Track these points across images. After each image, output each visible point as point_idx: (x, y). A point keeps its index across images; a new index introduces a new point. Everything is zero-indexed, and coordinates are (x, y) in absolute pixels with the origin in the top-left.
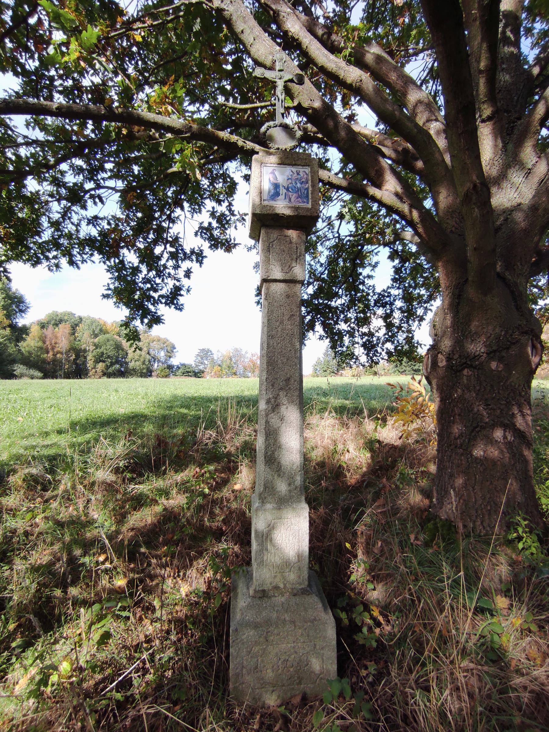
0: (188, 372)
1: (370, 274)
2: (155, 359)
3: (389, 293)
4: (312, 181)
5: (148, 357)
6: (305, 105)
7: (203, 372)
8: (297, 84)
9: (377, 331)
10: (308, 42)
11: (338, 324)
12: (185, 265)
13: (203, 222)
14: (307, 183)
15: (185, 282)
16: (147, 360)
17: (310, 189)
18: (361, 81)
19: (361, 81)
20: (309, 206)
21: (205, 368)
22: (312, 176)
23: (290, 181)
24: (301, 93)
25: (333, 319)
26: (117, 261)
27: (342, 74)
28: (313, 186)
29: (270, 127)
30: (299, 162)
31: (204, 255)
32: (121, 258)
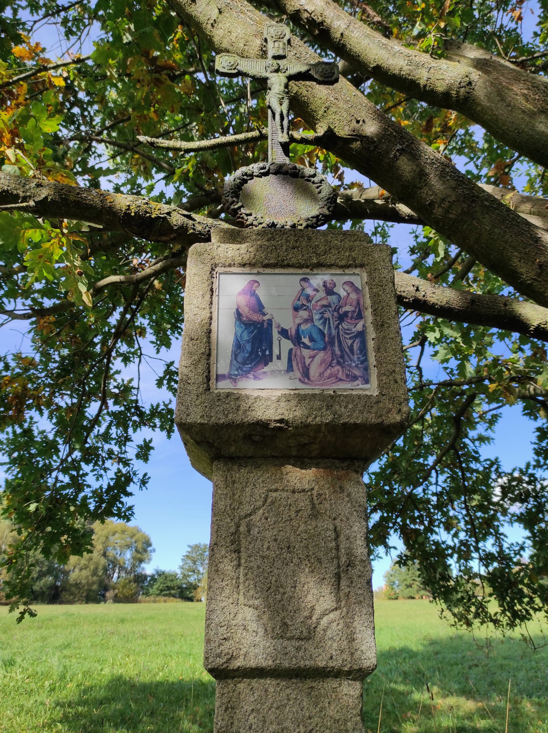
0: (169, 588)
1: (484, 434)
2: (114, 563)
3: (532, 475)
4: (375, 312)
5: (103, 561)
6: (343, 131)
7: (195, 587)
8: (320, 83)
9: (517, 553)
10: (343, 26)
11: (432, 532)
12: (140, 435)
13: (172, 363)
14: (360, 316)
15: (138, 466)
16: (101, 567)
17: (371, 334)
18: (470, 83)
19: (470, 83)
20: (372, 389)
21: (199, 580)
22: (374, 296)
23: (304, 314)
24: (332, 109)
25: (422, 523)
26: (19, 431)
27: (423, 76)
29: (251, 176)
30: (330, 258)
32: (26, 425)
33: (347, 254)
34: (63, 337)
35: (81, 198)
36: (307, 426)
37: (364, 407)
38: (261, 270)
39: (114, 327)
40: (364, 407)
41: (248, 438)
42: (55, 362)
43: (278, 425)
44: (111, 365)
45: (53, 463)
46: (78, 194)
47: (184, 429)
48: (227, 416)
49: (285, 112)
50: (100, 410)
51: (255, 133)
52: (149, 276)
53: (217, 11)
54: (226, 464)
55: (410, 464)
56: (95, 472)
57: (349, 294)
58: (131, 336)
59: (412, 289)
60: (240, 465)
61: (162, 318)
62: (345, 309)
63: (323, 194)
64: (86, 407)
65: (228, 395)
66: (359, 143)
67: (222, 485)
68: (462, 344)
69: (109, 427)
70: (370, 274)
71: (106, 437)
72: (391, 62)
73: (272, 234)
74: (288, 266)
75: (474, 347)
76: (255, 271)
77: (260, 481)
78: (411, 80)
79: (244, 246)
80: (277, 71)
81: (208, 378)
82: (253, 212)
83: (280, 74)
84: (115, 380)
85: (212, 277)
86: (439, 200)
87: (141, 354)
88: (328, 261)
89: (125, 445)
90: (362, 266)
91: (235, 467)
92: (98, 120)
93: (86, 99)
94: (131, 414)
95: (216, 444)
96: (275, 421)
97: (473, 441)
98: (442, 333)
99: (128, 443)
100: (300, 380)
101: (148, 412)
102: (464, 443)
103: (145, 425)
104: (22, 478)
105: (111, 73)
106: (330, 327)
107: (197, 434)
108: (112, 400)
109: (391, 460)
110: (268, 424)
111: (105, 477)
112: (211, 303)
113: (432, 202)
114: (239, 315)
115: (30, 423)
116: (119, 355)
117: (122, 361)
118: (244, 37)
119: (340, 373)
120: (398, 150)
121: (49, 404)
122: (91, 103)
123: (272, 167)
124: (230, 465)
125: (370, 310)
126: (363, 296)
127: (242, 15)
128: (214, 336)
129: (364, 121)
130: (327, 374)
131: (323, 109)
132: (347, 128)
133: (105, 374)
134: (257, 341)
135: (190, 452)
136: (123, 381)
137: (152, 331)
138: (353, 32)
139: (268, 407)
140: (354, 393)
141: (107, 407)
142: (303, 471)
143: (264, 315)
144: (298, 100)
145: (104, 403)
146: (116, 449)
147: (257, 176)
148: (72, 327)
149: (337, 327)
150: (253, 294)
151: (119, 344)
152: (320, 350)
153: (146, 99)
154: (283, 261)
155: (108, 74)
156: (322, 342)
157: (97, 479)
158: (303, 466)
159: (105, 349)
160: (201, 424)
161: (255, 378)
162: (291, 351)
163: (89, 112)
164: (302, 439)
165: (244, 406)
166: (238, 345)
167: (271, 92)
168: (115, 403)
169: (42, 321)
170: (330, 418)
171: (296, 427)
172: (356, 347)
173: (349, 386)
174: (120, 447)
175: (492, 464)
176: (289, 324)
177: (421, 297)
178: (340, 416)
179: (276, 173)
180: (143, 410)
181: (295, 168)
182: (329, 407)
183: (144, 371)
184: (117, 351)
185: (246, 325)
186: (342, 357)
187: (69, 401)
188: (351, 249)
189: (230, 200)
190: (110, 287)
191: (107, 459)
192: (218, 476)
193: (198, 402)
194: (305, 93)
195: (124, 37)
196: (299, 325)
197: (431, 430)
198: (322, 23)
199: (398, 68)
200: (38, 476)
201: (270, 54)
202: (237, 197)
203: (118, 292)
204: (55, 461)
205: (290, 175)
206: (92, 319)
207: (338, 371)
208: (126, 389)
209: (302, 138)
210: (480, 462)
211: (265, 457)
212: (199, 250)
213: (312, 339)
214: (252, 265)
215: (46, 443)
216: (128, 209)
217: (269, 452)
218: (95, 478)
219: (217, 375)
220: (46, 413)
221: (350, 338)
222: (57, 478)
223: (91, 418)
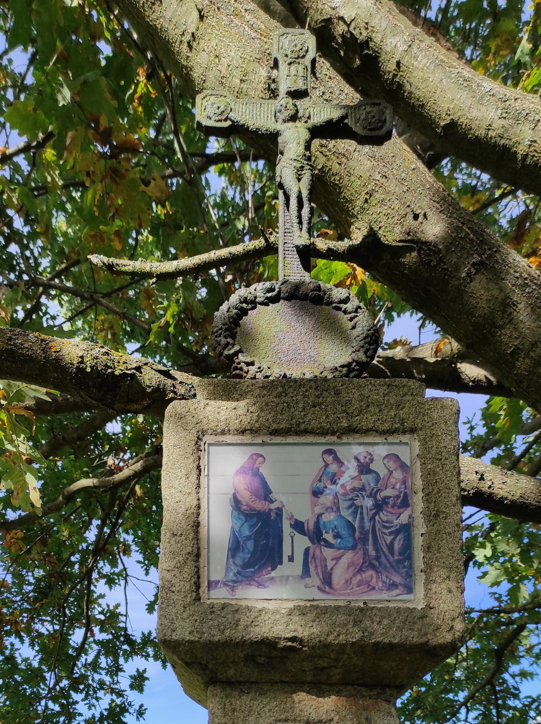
4: (427, 496)
6: (391, 236)
8: (362, 140)
12: (132, 665)
14: (405, 503)
15: (133, 696)
17: (420, 527)
22: (429, 476)
24: (378, 196)
28: (433, 516)
29: (254, 303)
30: (368, 420)
31: (136, 673)
32: (7, 652)
33: (392, 413)
34: (34, 554)
35: (15, 345)
36: (327, 646)
37: (404, 623)
38: (267, 439)
39: (92, 544)
40: (404, 623)
41: (251, 659)
42: (30, 584)
43: (290, 644)
44: (92, 588)
45: (41, 691)
46: (10, 339)
47: (169, 648)
48: (223, 632)
49: (305, 193)
50: (85, 638)
51: (259, 243)
52: (128, 479)
53: (196, 14)
54: (224, 689)
55: (437, 699)
56: (87, 702)
57: (391, 472)
58: (114, 555)
59: (475, 477)
60: (242, 691)
61: (149, 533)
62: (384, 494)
63: (358, 330)
64: (70, 635)
65: (224, 607)
66: (414, 254)
67: (219, 713)
68: (519, 563)
69: (97, 656)
70: (424, 443)
71: (95, 666)
72: (474, 113)
73: (283, 387)
74: (306, 432)
75: (535, 566)
76: (259, 440)
77: (266, 709)
78: (504, 146)
79: (242, 403)
80: (294, 118)
81: (198, 586)
82: (256, 359)
83: (298, 123)
84: (100, 605)
85: (199, 450)
86: (527, 345)
87: (127, 575)
88: (364, 425)
89: (117, 675)
90: (412, 431)
91: (236, 693)
92: (45, 262)
93: (26, 230)
94: (120, 643)
95: (210, 666)
96: (285, 639)
97: (513, 676)
98: (494, 549)
99: (119, 673)
100: (319, 588)
101: (139, 640)
102: (503, 679)
103: (137, 654)
104: (11, 706)
105: (53, 179)
106: (362, 518)
107: (186, 653)
108: (98, 627)
109: (415, 695)
110: (276, 643)
111: (98, 707)
112: (199, 486)
113: (517, 348)
114: (236, 503)
115: (12, 649)
116: (102, 576)
117: (106, 584)
118: (238, 62)
119: (374, 580)
120: (474, 264)
121: (29, 630)
122: (33, 236)
123: (283, 288)
124: (229, 691)
125: (420, 494)
126: (413, 475)
127: (236, 21)
128: (203, 530)
129: (425, 216)
130: (356, 580)
131: (363, 196)
132: (398, 229)
133: (87, 598)
134: (262, 539)
135: (180, 677)
136: (108, 606)
137: (137, 549)
138: (416, 58)
139: (276, 622)
140: (391, 605)
141: (93, 635)
142: (320, 699)
143: (272, 502)
144: (325, 183)
145: (89, 629)
146: (107, 679)
147: (262, 304)
148: (44, 543)
149: (373, 518)
150: (256, 473)
151: (101, 564)
152: (347, 549)
153: (101, 205)
154: (299, 425)
155: (49, 179)
156: (351, 539)
157: (90, 708)
158: (320, 693)
159: (84, 570)
160: (190, 642)
161: (260, 585)
162: (307, 550)
163: (32, 252)
164: (320, 662)
165: (244, 621)
166: (235, 547)
167: (283, 159)
168: (101, 631)
169: (9, 537)
170: (358, 636)
171: (313, 647)
172: (397, 546)
173: (385, 596)
174: (111, 677)
175: (534, 701)
176: (305, 515)
177: (485, 489)
178: (372, 634)
179: (288, 299)
180: (134, 638)
181: (318, 288)
182: (356, 623)
183: (132, 595)
184: (99, 572)
185: (246, 515)
186: (378, 558)
187: (50, 628)
188: (399, 406)
189: (223, 341)
190: (83, 493)
191: (99, 689)
192: (214, 703)
193: (185, 615)
194: (336, 168)
195: (59, 97)
196: (320, 515)
197: (465, 664)
198: (366, 43)
199: (485, 124)
200: (27, 704)
201: (283, 89)
202: (233, 336)
203: (93, 500)
204: (43, 689)
205: (309, 300)
206: (66, 533)
207: (372, 577)
208: (112, 617)
209: (329, 249)
210: (519, 699)
211: (273, 683)
212: (179, 410)
213: (337, 536)
214: (254, 431)
215: (31, 671)
216: (82, 362)
217: (278, 676)
218: (87, 706)
219: (209, 582)
220: (27, 640)
221: (390, 533)
222: (46, 706)
223: (76, 646)
